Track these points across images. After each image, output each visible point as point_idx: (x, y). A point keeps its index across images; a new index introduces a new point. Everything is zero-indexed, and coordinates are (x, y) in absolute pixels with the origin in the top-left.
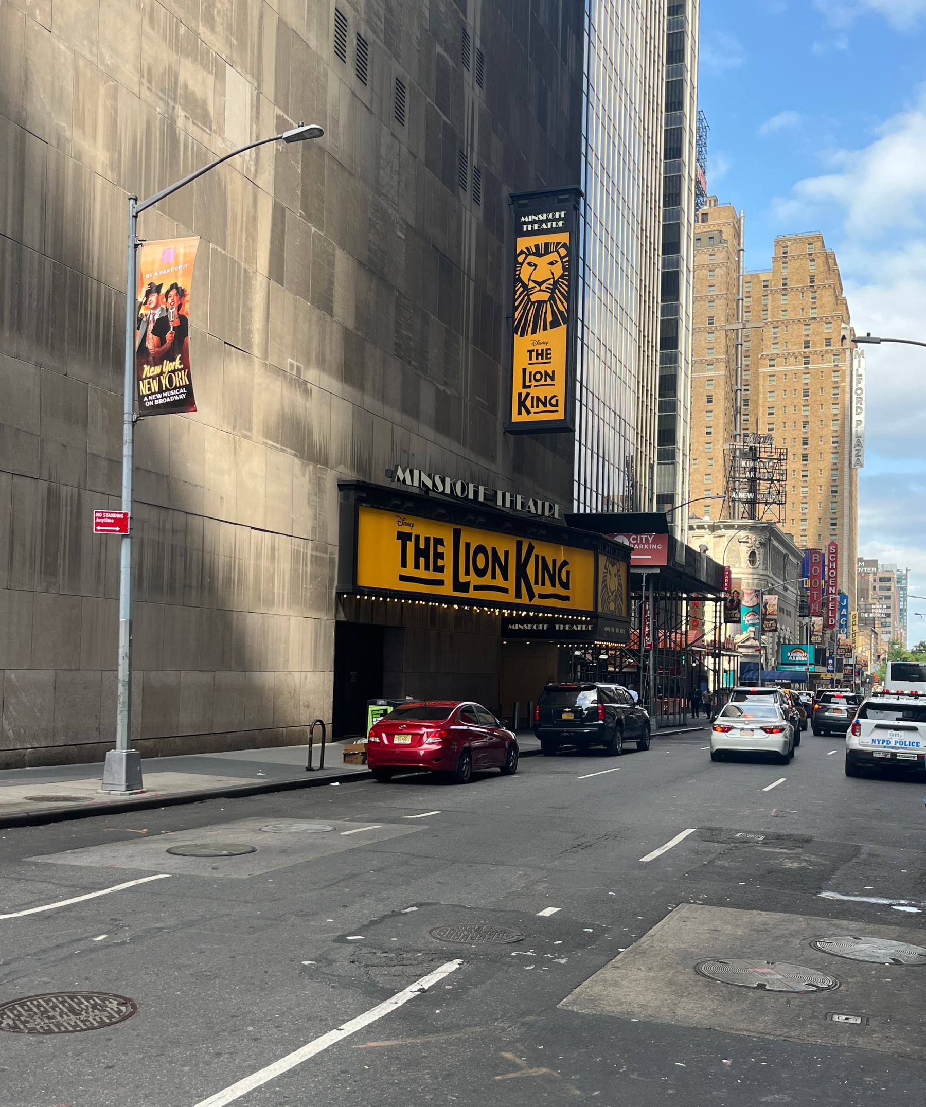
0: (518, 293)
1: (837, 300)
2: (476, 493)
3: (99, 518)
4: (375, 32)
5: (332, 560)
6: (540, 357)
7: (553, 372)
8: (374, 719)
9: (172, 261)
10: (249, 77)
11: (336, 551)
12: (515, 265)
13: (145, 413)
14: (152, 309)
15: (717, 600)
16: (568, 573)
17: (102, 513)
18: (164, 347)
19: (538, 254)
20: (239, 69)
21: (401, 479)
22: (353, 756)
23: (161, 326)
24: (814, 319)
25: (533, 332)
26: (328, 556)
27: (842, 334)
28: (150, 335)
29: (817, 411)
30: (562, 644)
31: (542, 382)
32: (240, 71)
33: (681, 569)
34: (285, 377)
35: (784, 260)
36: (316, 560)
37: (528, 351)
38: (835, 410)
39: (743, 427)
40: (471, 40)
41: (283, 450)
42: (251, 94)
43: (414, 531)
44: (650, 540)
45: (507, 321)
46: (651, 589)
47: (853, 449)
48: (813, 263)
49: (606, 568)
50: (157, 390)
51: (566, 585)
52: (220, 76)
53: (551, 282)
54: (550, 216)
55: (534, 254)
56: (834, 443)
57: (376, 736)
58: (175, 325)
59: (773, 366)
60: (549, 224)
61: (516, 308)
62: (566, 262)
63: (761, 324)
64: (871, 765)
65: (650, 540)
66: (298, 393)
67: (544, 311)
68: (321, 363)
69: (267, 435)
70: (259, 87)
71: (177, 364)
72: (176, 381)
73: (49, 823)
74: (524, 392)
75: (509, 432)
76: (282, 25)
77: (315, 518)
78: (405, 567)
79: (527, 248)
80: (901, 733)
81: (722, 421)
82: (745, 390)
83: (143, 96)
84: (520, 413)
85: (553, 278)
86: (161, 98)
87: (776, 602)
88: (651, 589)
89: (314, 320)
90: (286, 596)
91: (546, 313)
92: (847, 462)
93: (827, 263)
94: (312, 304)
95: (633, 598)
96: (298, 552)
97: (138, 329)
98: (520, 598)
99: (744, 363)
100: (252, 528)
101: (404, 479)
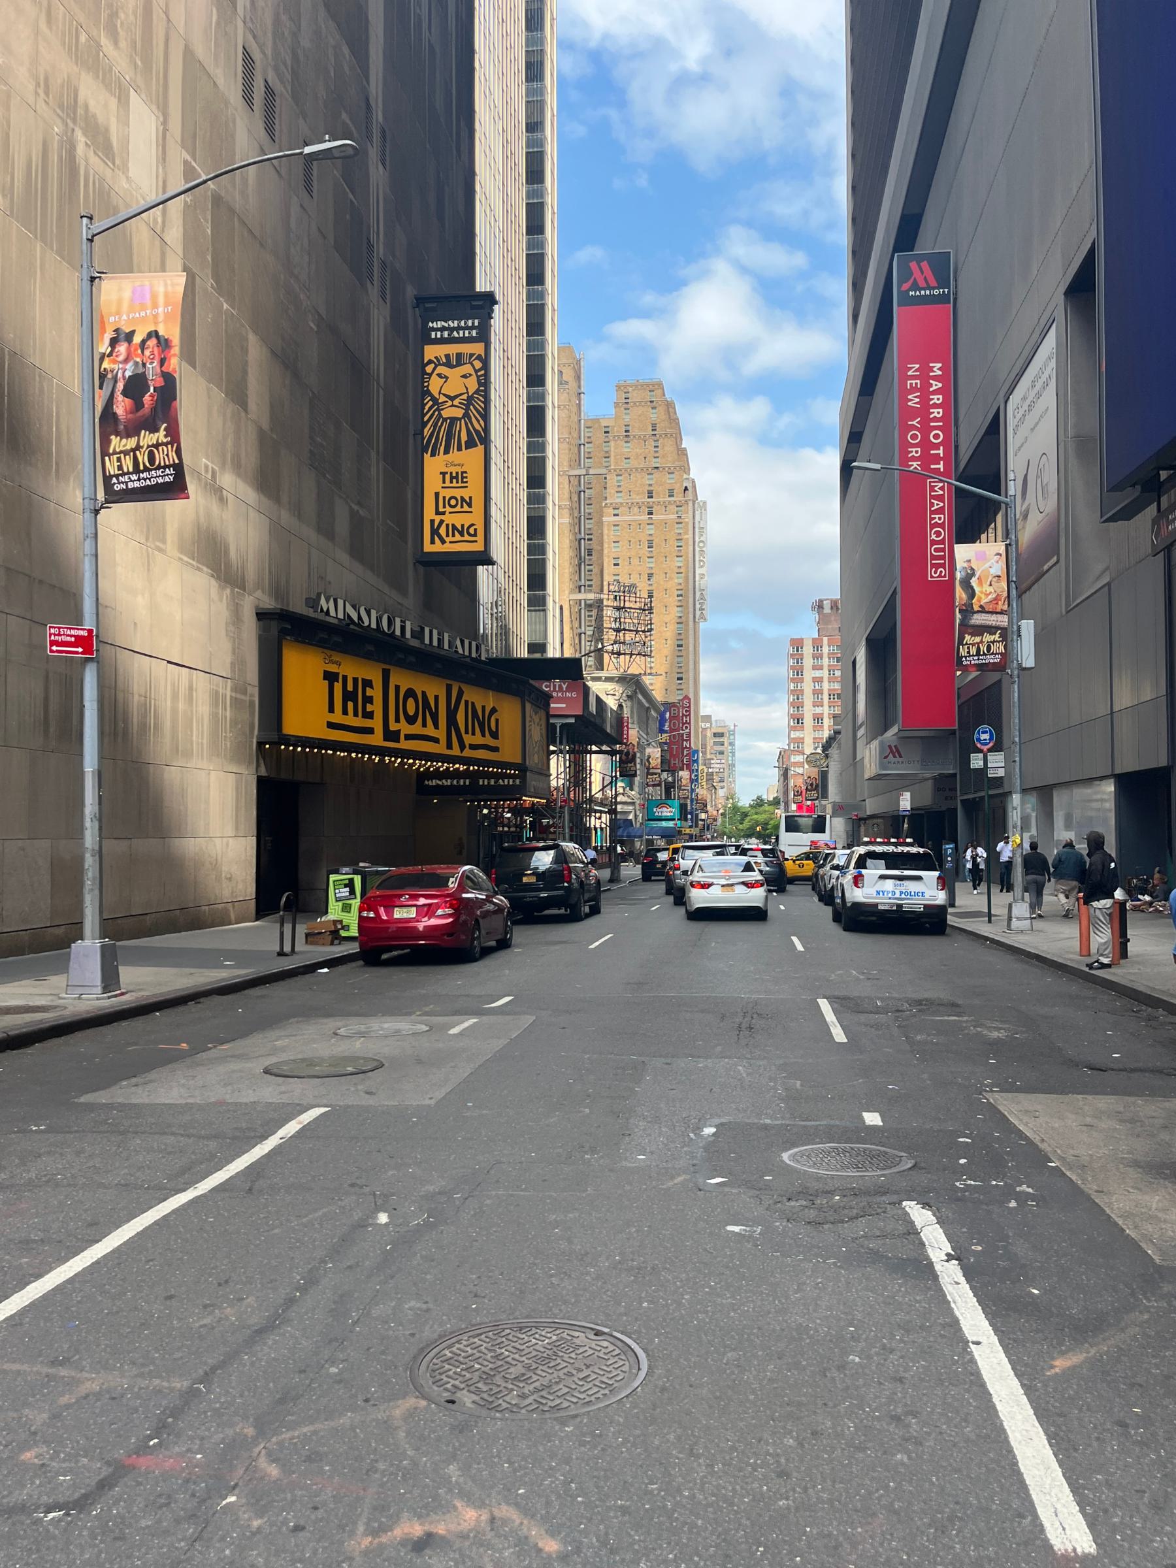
0: (427, 408)
1: (678, 450)
2: (403, 628)
3: (55, 635)
4: (282, 82)
5: (252, 703)
6: (454, 481)
7: (470, 498)
8: (337, 891)
9: (149, 303)
10: (154, 107)
11: (256, 691)
12: (422, 376)
13: (115, 498)
14: (120, 362)
15: (612, 753)
16: (497, 721)
17: (59, 628)
18: (140, 413)
19: (448, 364)
20: (143, 96)
21: (325, 610)
22: (319, 937)
23: (135, 388)
24: (657, 468)
25: (446, 452)
26: (248, 698)
27: (685, 485)
28: (119, 397)
29: (662, 563)
30: (472, 801)
31: (458, 508)
32: (145, 99)
33: (592, 719)
34: (200, 480)
35: (626, 406)
36: (235, 702)
37: (441, 473)
38: (679, 562)
39: (587, 578)
40: (374, 112)
41: (198, 569)
42: (157, 129)
43: (342, 671)
44: (564, 687)
45: (415, 440)
46: (564, 741)
47: (697, 603)
48: (654, 411)
49: (531, 717)
50: (131, 470)
51: (495, 735)
52: (123, 101)
53: (465, 396)
54: (462, 323)
55: (444, 364)
56: (678, 596)
57: (369, 910)
58: (158, 385)
59: (617, 515)
60: (461, 332)
61: (425, 424)
62: (481, 376)
63: (604, 471)
64: (874, 918)
65: (564, 687)
66: (214, 501)
67: (458, 429)
68: (237, 467)
69: (182, 550)
70: (165, 123)
71: (161, 436)
72: (159, 458)
73: (33, 1043)
74: (438, 519)
75: (418, 562)
76: (188, 52)
77: (234, 653)
78: (333, 712)
79: (436, 358)
80: (906, 883)
81: (567, 571)
82: (589, 540)
83: (39, 111)
84: (433, 542)
85: (468, 393)
86: (58, 115)
87: (659, 755)
88: (564, 741)
89: (229, 414)
90: (205, 746)
91: (460, 432)
92: (691, 616)
93: (669, 412)
94: (226, 396)
95: (554, 752)
96: (217, 692)
97: (101, 387)
98: (451, 749)
99: (587, 511)
100: (169, 662)
101: (328, 609)
